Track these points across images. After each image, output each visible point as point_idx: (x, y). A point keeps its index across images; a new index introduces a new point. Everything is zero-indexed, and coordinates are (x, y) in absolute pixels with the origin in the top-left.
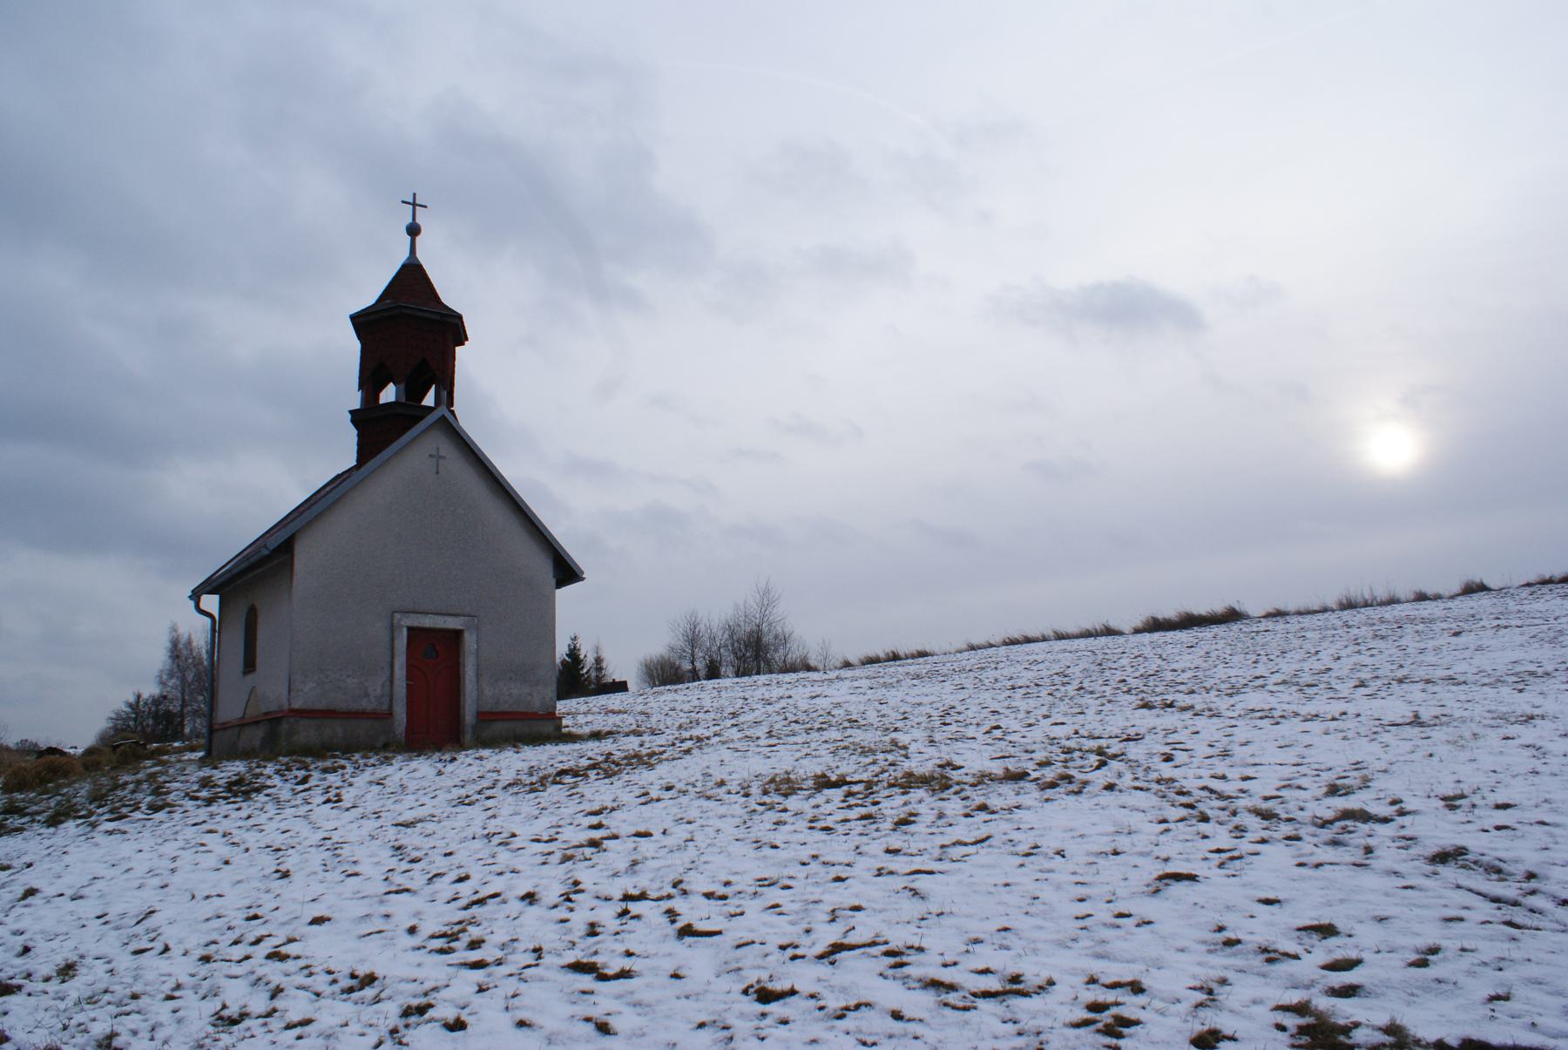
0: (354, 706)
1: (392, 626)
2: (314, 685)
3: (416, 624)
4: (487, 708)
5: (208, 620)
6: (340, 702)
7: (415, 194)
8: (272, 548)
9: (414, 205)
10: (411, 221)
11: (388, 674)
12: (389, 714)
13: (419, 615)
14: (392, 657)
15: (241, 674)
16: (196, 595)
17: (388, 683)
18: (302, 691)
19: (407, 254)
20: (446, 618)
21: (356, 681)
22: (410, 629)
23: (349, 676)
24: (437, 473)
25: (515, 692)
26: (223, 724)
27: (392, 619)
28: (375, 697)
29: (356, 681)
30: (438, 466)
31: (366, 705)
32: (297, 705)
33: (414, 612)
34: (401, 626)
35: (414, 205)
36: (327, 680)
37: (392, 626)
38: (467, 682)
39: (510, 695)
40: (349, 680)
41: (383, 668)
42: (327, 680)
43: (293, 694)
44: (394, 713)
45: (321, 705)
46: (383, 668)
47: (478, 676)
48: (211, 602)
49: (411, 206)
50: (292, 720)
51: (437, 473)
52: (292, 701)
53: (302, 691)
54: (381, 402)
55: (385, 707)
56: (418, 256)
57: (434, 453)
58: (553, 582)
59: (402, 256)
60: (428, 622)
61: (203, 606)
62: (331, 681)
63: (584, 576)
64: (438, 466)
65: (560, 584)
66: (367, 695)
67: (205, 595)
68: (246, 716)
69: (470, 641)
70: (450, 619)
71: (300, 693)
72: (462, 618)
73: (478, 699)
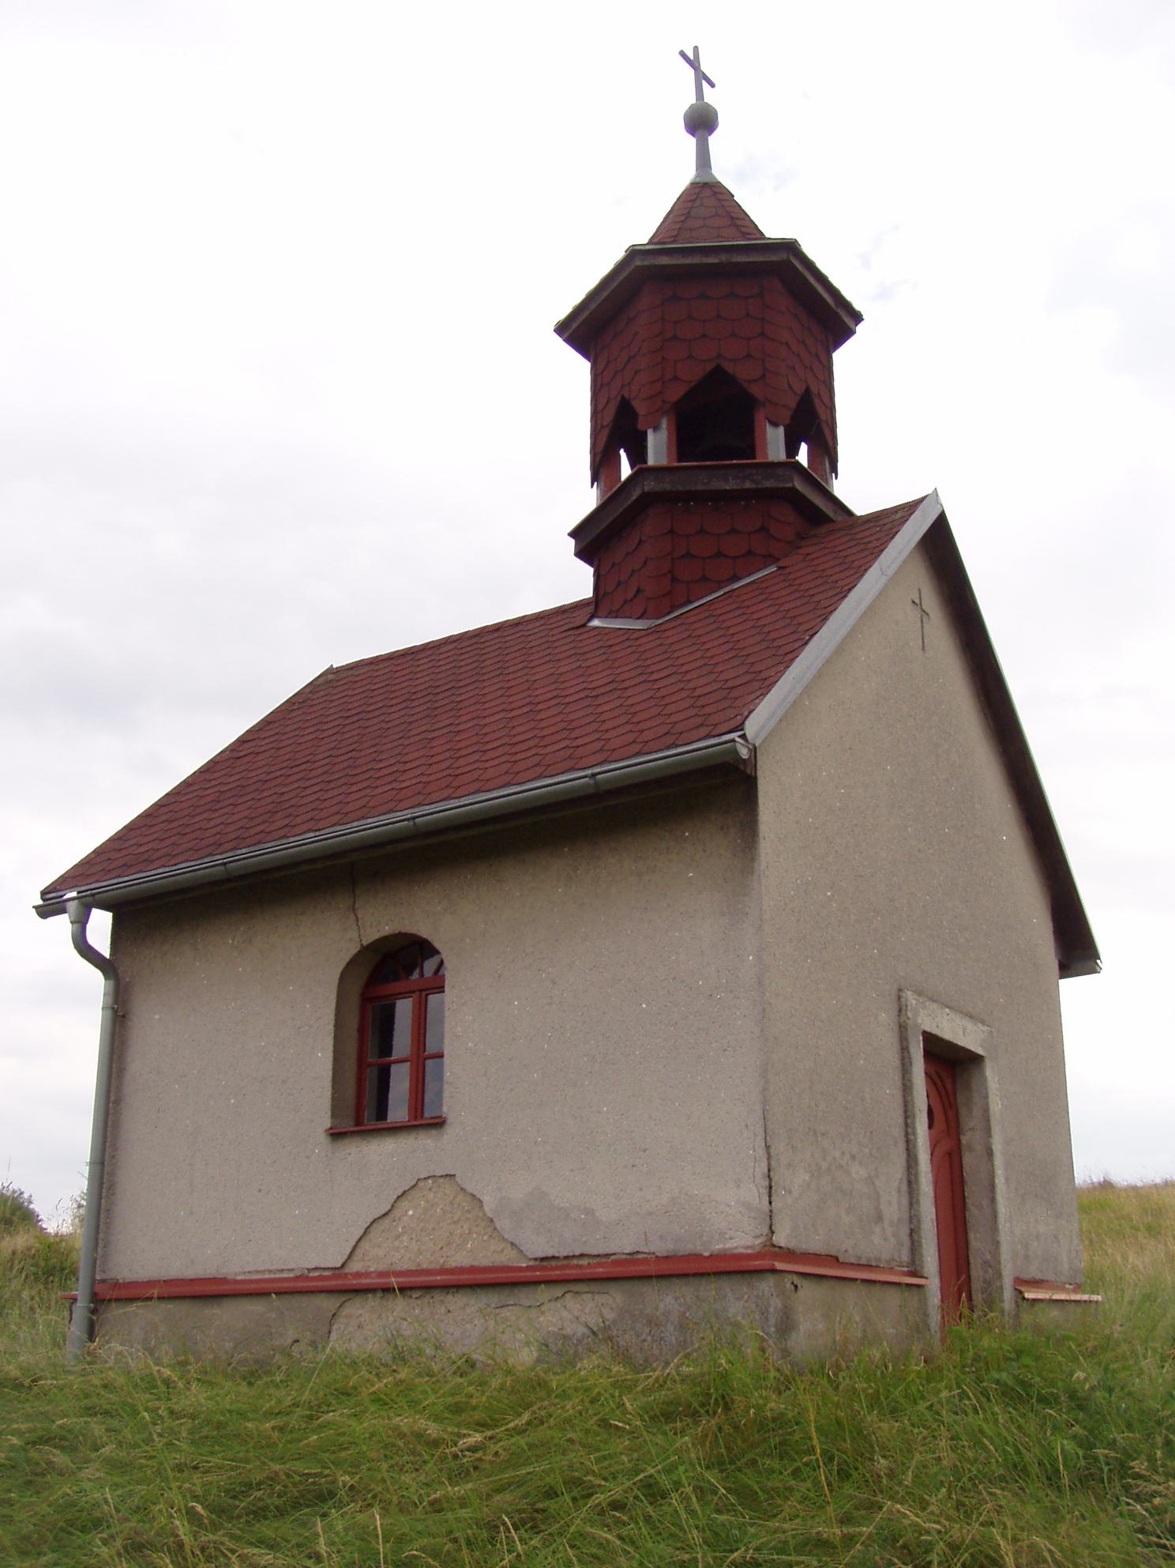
10: (694, 101)
15: (322, 1138)
55: (905, 1257)
59: (685, 175)
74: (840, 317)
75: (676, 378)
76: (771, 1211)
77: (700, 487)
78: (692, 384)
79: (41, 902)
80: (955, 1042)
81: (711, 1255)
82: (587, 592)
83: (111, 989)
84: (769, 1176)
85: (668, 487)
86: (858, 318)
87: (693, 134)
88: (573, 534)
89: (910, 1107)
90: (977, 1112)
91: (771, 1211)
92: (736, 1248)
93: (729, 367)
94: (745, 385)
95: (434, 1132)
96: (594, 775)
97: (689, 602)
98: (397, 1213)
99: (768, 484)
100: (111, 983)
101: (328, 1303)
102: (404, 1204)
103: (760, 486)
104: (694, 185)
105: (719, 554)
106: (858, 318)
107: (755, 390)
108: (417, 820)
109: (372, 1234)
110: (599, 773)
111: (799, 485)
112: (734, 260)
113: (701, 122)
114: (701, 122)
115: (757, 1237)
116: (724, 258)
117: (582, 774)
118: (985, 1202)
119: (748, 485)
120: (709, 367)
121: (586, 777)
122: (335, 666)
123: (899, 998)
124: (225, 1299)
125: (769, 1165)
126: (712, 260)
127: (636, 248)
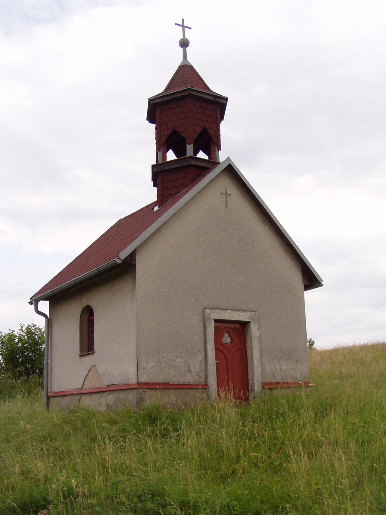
0: (182, 380)
1: (204, 319)
2: (154, 364)
3: (220, 317)
4: (268, 380)
5: (43, 318)
6: (174, 378)
7: (183, 19)
8: (123, 259)
9: (183, 26)
10: (182, 37)
11: (203, 355)
12: (205, 386)
13: (221, 311)
14: (205, 342)
15: (78, 357)
16: (35, 301)
17: (203, 362)
18: (146, 368)
19: (181, 60)
20: (239, 313)
21: (182, 360)
22: (216, 321)
23: (177, 357)
24: (226, 206)
25: (284, 367)
26: (55, 393)
27: (204, 315)
28: (195, 372)
29: (182, 360)
30: (226, 200)
31: (189, 379)
32: (143, 380)
33: (217, 308)
34: (210, 319)
35: (183, 26)
36: (163, 360)
37: (204, 319)
38: (255, 360)
39: (281, 370)
40: (177, 360)
41: (199, 351)
42: (163, 360)
43: (140, 371)
44: (209, 385)
45: (160, 379)
46: (199, 351)
47: (261, 356)
48: (44, 306)
49: (185, 25)
50: (141, 391)
51: (226, 206)
52: (139, 377)
53: (146, 368)
54: (168, 160)
55: (202, 380)
56: (188, 60)
57: (224, 192)
58: (303, 287)
59: (179, 61)
60: (227, 316)
61: (40, 309)
62: (165, 361)
63: (322, 283)
64: (226, 200)
65: (307, 287)
66: (190, 371)
67: (41, 301)
68: (84, 388)
69: (254, 331)
70: (241, 313)
71: (146, 370)
72: (249, 313)
73: (262, 373)
74: (218, 102)
75: (163, 135)
76: (138, 374)
77: (167, 168)
78: (168, 136)
79: (30, 301)
80: (232, 319)
81: (130, 384)
82: (155, 199)
83: (47, 321)
84: (137, 365)
85: (159, 170)
86: (226, 99)
87: (182, 47)
88: (152, 181)
89: (206, 341)
90: (249, 336)
91: (138, 374)
92: (133, 383)
93: (177, 129)
94: (181, 134)
95: (93, 355)
96: (98, 269)
97: (167, 202)
98: (89, 374)
99: (184, 164)
100: (47, 319)
101: (78, 397)
102: (90, 373)
103: (182, 165)
104: (181, 67)
105: (174, 186)
106: (226, 99)
107: (184, 135)
108: (77, 280)
109: (86, 380)
110: (99, 268)
111: (193, 162)
112: (176, 96)
113: (184, 44)
114: (184, 44)
115: (136, 380)
116: (173, 97)
117: (96, 269)
118: (251, 362)
119: (179, 165)
120: (172, 130)
121: (96, 269)
122: (122, 218)
123: (204, 312)
124: (66, 396)
125: (137, 362)
126: (170, 98)
127: (150, 99)
